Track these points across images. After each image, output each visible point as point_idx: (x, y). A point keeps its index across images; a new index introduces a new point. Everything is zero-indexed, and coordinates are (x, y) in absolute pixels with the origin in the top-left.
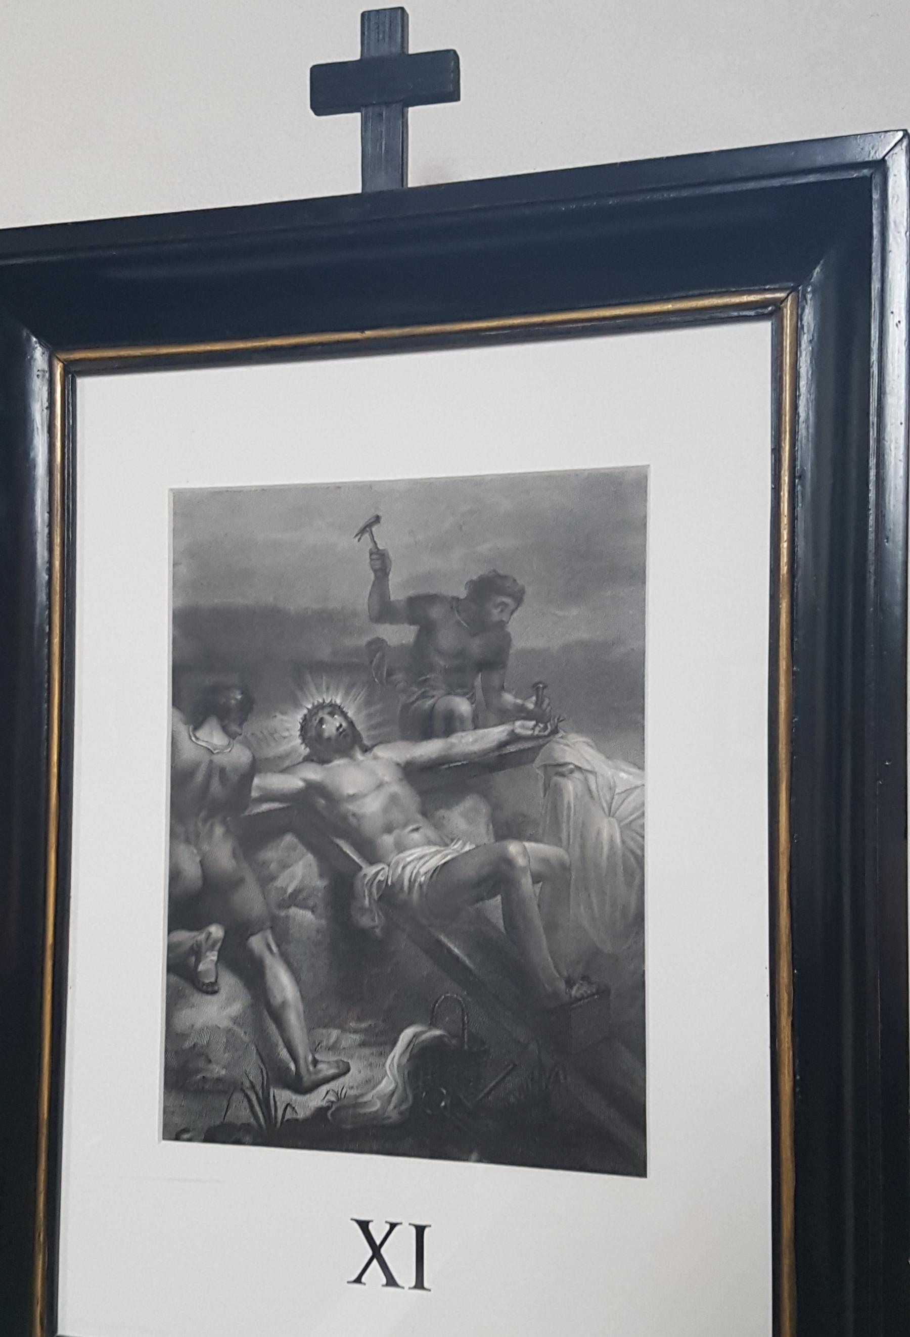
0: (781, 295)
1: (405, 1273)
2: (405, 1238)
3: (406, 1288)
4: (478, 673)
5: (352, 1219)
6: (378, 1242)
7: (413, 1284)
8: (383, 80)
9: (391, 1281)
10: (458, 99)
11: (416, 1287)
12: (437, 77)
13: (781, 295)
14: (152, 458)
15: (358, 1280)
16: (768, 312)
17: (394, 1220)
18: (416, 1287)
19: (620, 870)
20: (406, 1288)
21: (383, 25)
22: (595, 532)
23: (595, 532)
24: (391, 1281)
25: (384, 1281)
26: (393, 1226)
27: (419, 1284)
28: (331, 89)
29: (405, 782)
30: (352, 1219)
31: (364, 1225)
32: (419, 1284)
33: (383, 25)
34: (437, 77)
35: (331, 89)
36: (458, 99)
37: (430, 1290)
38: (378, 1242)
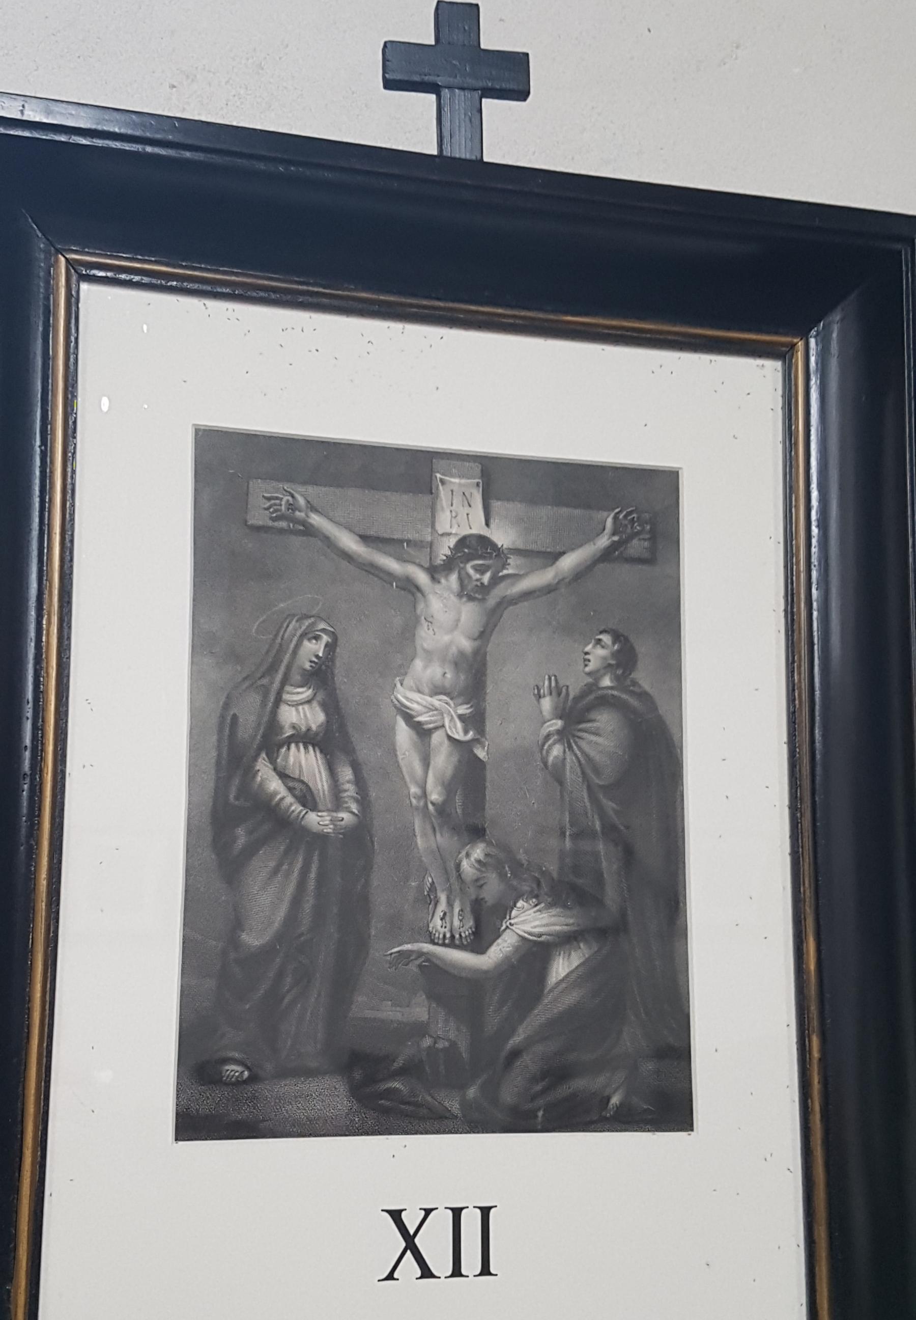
1: (440, 1263)
2: (442, 1221)
3: (471, 1207)
4: (561, 718)
9: (427, 1273)
10: (527, 55)
12: (510, 77)
14: (160, 374)
15: (390, 1277)
16: (783, 354)
19: (538, 908)
20: (471, 1207)
21: (457, 21)
25: (419, 1273)
26: (428, 1212)
27: (486, 1270)
28: (404, 69)
31: (396, 1215)
32: (486, 1270)
33: (457, 21)
34: (510, 77)
35: (404, 69)
36: (527, 55)
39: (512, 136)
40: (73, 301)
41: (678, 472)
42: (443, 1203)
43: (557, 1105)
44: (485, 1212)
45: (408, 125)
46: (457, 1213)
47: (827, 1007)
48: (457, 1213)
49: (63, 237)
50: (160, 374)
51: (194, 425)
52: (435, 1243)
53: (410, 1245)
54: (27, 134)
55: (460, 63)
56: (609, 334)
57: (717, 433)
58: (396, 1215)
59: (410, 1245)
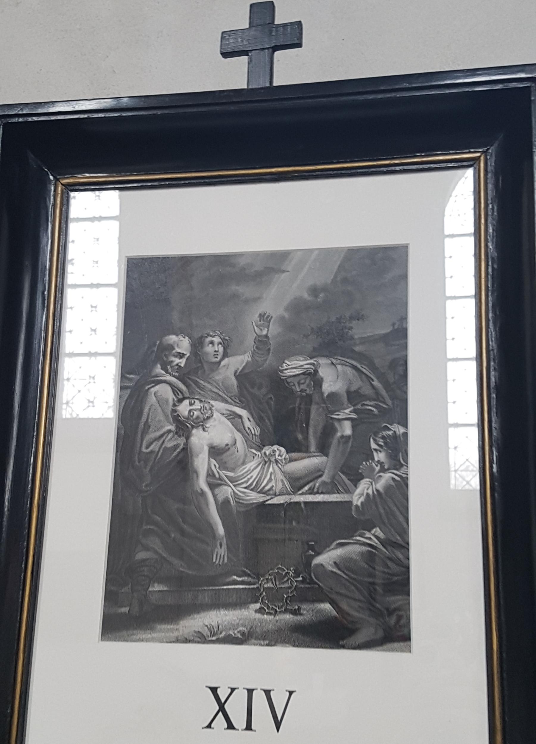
0: (479, 154)
2: (241, 696)
5: (207, 687)
6: (220, 713)
7: (244, 726)
8: (268, 33)
9: (231, 726)
11: (253, 690)
12: (291, 37)
13: (479, 154)
15: (209, 726)
17: (233, 686)
18: (253, 690)
20: (240, 730)
22: (154, 290)
23: (379, 272)
24: (231, 726)
26: (233, 690)
27: (249, 727)
29: (160, 585)
30: (207, 687)
31: (214, 690)
32: (249, 727)
34: (291, 37)
37: (255, 731)
38: (220, 713)
39: (291, 69)
40: (462, 164)
41: (407, 247)
42: (242, 685)
43: (331, 634)
44: (268, 693)
45: (234, 76)
46: (250, 692)
47: (21, 587)
48: (250, 692)
49: (60, 171)
50: (99, 234)
51: (126, 256)
52: (236, 709)
53: (222, 708)
54: (130, 114)
55: (268, 33)
56: (309, 176)
57: (438, 222)
58: (214, 690)
59: (222, 708)
